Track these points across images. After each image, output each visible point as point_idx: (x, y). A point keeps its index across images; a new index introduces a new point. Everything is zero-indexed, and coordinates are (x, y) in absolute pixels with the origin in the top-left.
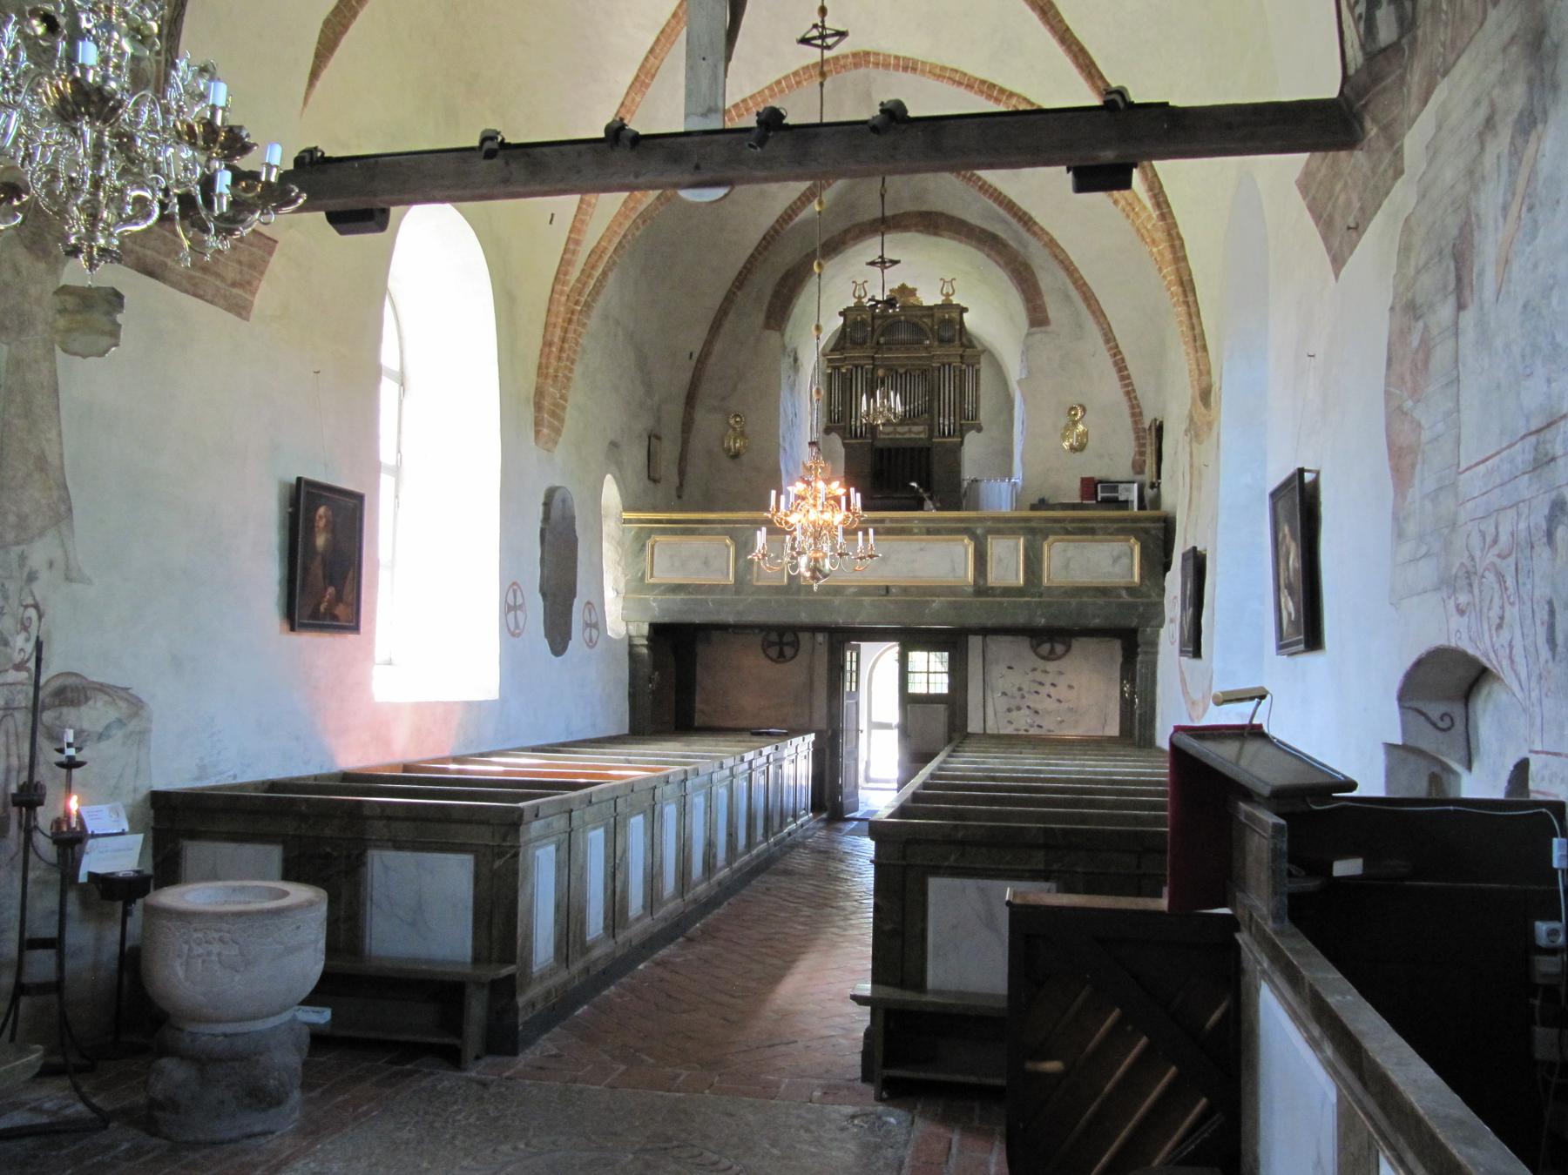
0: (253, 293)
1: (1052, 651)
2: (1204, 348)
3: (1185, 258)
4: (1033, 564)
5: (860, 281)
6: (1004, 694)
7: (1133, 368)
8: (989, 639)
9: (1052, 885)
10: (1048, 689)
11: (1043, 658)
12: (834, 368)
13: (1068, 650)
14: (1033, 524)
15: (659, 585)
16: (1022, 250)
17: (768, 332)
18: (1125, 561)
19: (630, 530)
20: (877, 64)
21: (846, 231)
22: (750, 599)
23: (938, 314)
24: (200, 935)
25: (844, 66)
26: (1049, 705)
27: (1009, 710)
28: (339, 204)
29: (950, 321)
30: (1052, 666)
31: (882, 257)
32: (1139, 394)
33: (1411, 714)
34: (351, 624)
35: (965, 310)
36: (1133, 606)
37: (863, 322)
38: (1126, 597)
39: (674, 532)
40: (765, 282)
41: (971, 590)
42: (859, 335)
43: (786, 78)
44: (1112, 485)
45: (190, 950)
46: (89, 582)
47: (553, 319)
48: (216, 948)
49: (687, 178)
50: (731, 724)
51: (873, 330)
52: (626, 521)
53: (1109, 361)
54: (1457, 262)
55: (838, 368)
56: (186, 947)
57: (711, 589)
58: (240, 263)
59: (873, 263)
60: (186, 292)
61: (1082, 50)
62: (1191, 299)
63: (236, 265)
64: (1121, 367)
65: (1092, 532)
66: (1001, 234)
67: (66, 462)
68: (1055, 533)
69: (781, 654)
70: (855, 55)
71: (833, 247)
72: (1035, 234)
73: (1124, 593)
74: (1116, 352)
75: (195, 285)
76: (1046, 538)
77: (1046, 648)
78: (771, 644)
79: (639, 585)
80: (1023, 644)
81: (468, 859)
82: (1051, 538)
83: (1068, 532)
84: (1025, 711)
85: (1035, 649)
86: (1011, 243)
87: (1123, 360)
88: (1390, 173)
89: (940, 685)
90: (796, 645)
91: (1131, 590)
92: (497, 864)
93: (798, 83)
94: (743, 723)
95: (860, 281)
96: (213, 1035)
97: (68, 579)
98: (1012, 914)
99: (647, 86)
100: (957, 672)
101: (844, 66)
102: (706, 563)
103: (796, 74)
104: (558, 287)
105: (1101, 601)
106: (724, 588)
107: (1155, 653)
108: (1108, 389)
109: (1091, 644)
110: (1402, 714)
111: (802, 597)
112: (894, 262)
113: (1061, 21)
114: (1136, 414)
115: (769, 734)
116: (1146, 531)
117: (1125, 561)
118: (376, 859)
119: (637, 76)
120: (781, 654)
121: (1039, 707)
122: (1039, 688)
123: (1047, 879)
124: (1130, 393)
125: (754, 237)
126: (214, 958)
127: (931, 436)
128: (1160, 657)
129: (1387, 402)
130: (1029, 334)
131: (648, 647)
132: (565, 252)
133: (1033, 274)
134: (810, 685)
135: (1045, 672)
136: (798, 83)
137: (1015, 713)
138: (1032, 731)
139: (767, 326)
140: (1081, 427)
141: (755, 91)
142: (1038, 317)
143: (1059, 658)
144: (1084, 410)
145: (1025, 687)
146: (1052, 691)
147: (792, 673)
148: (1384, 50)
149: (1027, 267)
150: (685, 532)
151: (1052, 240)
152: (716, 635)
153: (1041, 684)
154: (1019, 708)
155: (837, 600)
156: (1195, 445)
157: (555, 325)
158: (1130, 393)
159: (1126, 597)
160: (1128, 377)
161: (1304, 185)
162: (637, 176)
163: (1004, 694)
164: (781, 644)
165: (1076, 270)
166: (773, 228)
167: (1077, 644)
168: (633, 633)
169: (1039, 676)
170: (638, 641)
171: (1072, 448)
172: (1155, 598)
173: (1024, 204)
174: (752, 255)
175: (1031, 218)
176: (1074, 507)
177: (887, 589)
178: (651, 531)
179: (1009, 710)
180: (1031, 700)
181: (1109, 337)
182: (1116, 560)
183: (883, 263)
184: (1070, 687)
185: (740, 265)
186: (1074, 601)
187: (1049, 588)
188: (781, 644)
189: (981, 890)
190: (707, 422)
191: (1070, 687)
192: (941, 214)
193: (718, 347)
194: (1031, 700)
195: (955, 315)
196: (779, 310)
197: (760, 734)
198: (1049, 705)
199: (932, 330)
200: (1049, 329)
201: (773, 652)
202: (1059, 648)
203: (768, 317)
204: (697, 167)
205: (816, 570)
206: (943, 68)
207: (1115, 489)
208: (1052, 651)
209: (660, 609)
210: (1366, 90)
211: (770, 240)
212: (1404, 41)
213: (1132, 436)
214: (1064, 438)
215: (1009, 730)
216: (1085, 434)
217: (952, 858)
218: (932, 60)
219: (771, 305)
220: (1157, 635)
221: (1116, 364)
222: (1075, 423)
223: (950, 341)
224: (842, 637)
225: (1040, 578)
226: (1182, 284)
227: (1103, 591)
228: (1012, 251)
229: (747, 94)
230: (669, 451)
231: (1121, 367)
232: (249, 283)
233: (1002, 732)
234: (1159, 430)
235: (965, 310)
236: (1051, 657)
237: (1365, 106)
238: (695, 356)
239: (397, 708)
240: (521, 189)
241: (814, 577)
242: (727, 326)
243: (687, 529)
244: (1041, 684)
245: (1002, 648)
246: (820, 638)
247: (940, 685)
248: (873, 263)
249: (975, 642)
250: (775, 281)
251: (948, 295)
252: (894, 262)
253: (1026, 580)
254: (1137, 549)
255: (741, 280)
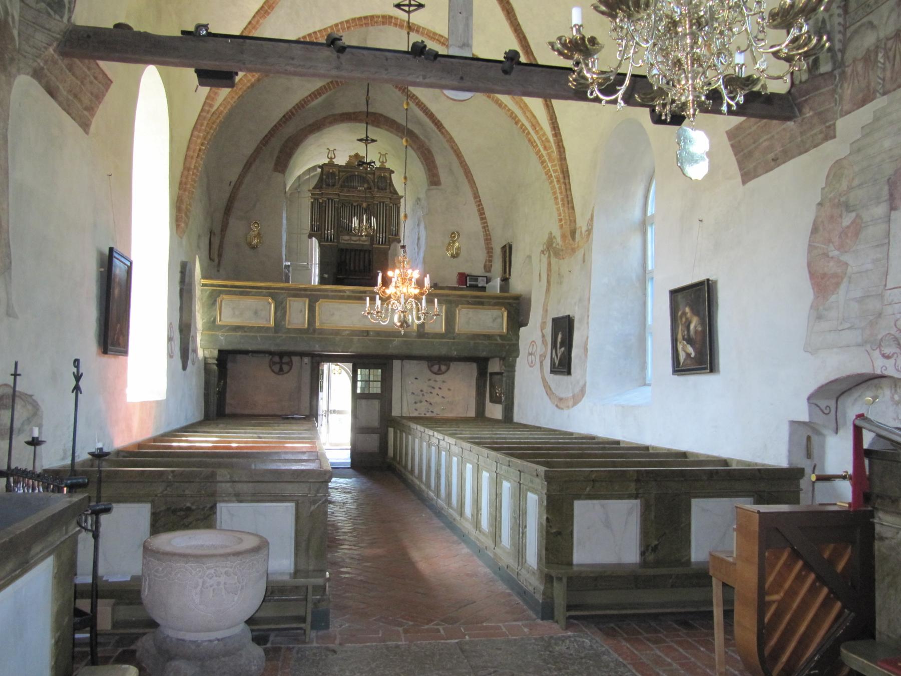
0: (93, 115)
1: (440, 369)
2: (573, 208)
3: (565, 159)
4: (450, 320)
5: (331, 149)
6: (413, 393)
7: (488, 214)
8: (406, 362)
9: (751, 499)
10: (436, 391)
11: (435, 373)
12: (315, 199)
13: (448, 369)
14: (450, 298)
15: (224, 326)
16: (427, 141)
17: (277, 173)
18: (499, 320)
19: (206, 291)
20: (396, 25)
21: (325, 118)
22: (284, 336)
23: (377, 174)
24: (213, 571)
25: (376, 22)
26: (438, 399)
27: (416, 403)
28: (209, 64)
29: (384, 177)
30: (439, 378)
31: (367, 137)
32: (490, 228)
33: (813, 406)
34: (125, 352)
35: (393, 172)
36: (503, 345)
37: (333, 174)
38: (499, 341)
39: (235, 293)
40: (277, 143)
41: (415, 334)
42: (331, 181)
43: (342, 23)
44: (475, 278)
45: (204, 583)
46: (16, 317)
47: (191, 153)
48: (222, 579)
49: (456, 83)
50: (247, 412)
51: (339, 179)
52: (203, 285)
53: (476, 209)
54: (890, 186)
55: (318, 199)
56: (200, 581)
57: (260, 329)
58: (92, 94)
59: (361, 140)
60: (64, 109)
61: (525, 37)
62: (567, 181)
63: (89, 95)
64: (482, 213)
65: (482, 304)
66: (416, 131)
67: (10, 226)
68: (462, 304)
69: (281, 370)
70: (383, 17)
71: (317, 127)
72: (442, 133)
73: (498, 338)
74: (479, 204)
75: (69, 105)
76: (457, 306)
77: (436, 367)
78: (275, 363)
79: (212, 325)
80: (424, 365)
81: (291, 506)
82: (460, 306)
83: (469, 303)
84: (424, 403)
85: (430, 367)
86: (422, 137)
87: (483, 209)
88: (820, 136)
89: (376, 388)
90: (290, 364)
91: (502, 336)
92: (313, 508)
93: (348, 28)
94: (256, 412)
95: (331, 149)
96: (210, 641)
97: (8, 314)
98: (760, 517)
99: (269, 14)
100: (386, 381)
101: (376, 22)
102: (256, 313)
103: (347, 22)
104: (196, 133)
105: (486, 342)
106: (267, 329)
107: (514, 371)
108: (473, 224)
109: (461, 366)
110: (810, 407)
111: (316, 336)
112: (373, 141)
113: (516, 19)
114: (488, 239)
115: (293, 418)
116: (510, 304)
117: (499, 320)
118: (224, 510)
119: (262, 7)
120: (281, 370)
121: (432, 401)
122: (433, 391)
123: (636, 498)
124: (485, 227)
125: (277, 115)
126: (222, 586)
127: (372, 243)
128: (516, 373)
129: (809, 252)
130: (429, 190)
131: (217, 365)
132: (202, 110)
133: (433, 156)
134: (299, 389)
135: (435, 381)
136: (348, 28)
137: (418, 405)
138: (428, 415)
139: (276, 169)
140: (457, 244)
141: (322, 28)
142: (434, 180)
143: (443, 373)
144: (459, 235)
145: (425, 391)
146: (439, 392)
147: (287, 382)
148: (822, 75)
149: (430, 152)
150: (241, 294)
151: (451, 138)
152: (239, 357)
153: (433, 388)
154: (421, 402)
155: (338, 338)
156: (554, 260)
157: (192, 157)
158: (485, 227)
159: (499, 341)
160: (485, 218)
161: (732, 135)
162: (424, 78)
163: (413, 393)
164: (281, 363)
165: (462, 156)
166: (291, 111)
167: (453, 365)
168: (208, 355)
169: (432, 383)
170: (210, 361)
171: (453, 256)
172: (514, 342)
173: (439, 116)
174: (275, 126)
175: (441, 125)
176: (454, 289)
177: (368, 332)
178: (220, 292)
179: (416, 403)
180: (428, 397)
181: (476, 196)
182: (494, 320)
183: (367, 141)
184: (449, 390)
185: (266, 131)
186: (472, 342)
187: (459, 334)
188: (281, 363)
189: (603, 506)
190: (236, 227)
191: (449, 390)
192: (381, 115)
193: (247, 180)
194: (428, 397)
195: (387, 175)
196: (283, 162)
197: (288, 418)
198: (438, 399)
199: (374, 182)
200: (439, 187)
201: (276, 368)
202: (443, 368)
203: (276, 165)
204: (462, 78)
205: (404, 322)
206: (435, 34)
207: (476, 280)
208: (440, 369)
209: (225, 341)
210: (807, 92)
211: (287, 118)
212: (836, 72)
213: (485, 251)
214: (448, 250)
215: (415, 414)
216: (459, 249)
217: (588, 489)
218: (430, 28)
219: (278, 157)
220: (515, 361)
221: (479, 211)
222: (454, 242)
223: (384, 189)
224: (317, 360)
225: (454, 329)
226: (563, 172)
227: (488, 337)
228: (425, 143)
229: (317, 29)
230: (216, 241)
231: (482, 213)
232: (92, 109)
233: (411, 415)
234: (507, 251)
235: (393, 172)
236: (439, 372)
237: (806, 101)
238: (233, 184)
239: (134, 404)
240: (498, 88)
241: (401, 326)
242: (253, 168)
243: (244, 292)
244: (433, 388)
245: (412, 367)
246: (306, 360)
247: (376, 388)
248: (361, 140)
249: (397, 364)
250: (283, 144)
251: (331, 159)
252: (373, 141)
253: (309, 324)
254: (505, 314)
255: (266, 141)
